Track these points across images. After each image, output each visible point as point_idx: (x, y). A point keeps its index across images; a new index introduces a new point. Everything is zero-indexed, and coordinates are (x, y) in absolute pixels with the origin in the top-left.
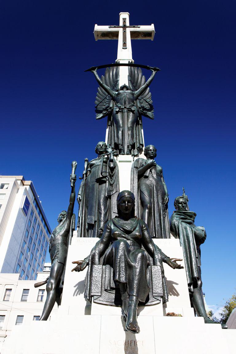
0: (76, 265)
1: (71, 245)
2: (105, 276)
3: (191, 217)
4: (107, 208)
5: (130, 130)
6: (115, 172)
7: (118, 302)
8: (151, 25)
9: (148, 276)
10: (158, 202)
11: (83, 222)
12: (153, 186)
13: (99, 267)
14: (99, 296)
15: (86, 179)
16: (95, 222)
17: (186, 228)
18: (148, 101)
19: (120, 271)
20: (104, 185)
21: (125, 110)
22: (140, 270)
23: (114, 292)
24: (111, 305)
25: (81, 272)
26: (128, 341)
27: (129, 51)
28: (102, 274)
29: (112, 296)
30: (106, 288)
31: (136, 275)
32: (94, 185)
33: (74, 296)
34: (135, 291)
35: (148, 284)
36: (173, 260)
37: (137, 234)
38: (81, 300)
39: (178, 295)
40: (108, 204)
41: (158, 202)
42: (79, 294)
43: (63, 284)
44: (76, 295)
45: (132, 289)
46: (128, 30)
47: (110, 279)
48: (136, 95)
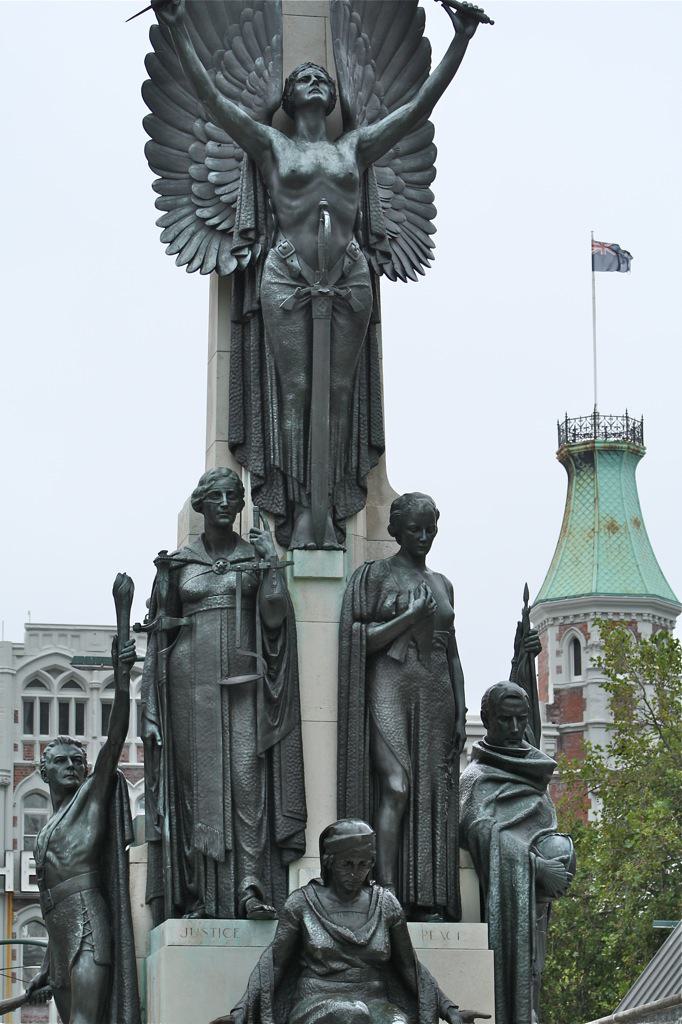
16: (227, 852)
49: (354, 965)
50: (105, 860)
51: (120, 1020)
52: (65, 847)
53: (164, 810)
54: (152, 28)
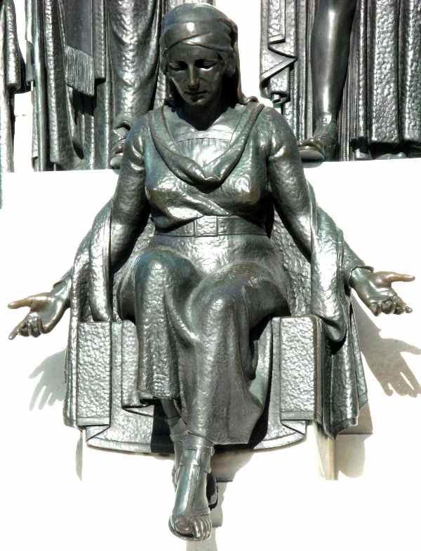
0: (26, 310)
1: (11, 168)
2: (123, 363)
4: (150, 8)
7: (162, 443)
11: (51, 65)
13: (100, 330)
14: (105, 427)
16: (99, 82)
23: (150, 411)
24: (146, 454)
25: (42, 336)
28: (111, 356)
29: (145, 424)
30: (126, 403)
33: (32, 406)
34: (201, 420)
44: (41, 407)
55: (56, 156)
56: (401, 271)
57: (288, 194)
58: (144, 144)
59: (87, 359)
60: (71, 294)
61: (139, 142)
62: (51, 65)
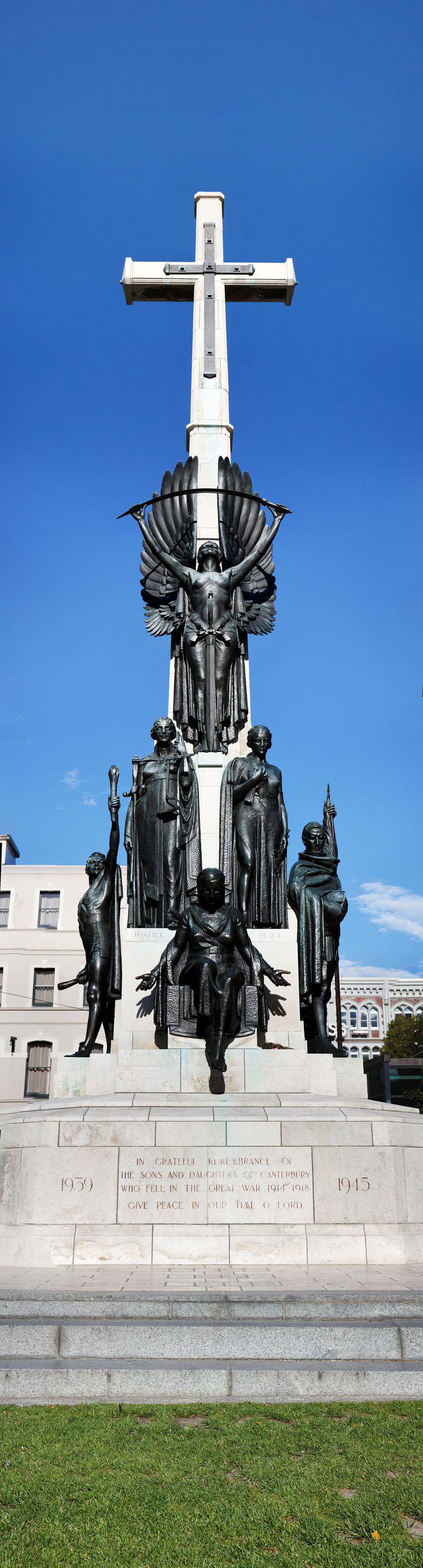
3: (329, 866)
5: (220, 688)
6: (192, 796)
8: (284, 261)
9: (239, 1002)
10: (267, 855)
11: (139, 890)
12: (261, 823)
15: (137, 804)
16: (161, 896)
17: (311, 902)
18: (168, 501)
19: (203, 1002)
20: (173, 822)
21: (211, 638)
22: (228, 1000)
25: (79, 1046)
26: (314, 1279)
27: (221, 388)
31: (223, 1006)
32: (154, 823)
33: (137, 1017)
35: (238, 1012)
36: (277, 973)
37: (227, 936)
38: (148, 1024)
39: (283, 1014)
40: (180, 860)
41: (267, 855)
42: (145, 1016)
43: (287, 837)
44: (141, 1017)
45: (218, 1023)
46: (200, 260)
47: (320, 928)
48: (235, 578)
49: (214, 945)
50: (109, 908)
51: (6, 1363)
52: (196, 957)
53: (133, 879)
54: (225, 1071)
55: (139, 923)
56: (285, 970)
57: (179, 571)
58: (188, 918)
59: (170, 999)
60: (159, 975)
61: (243, 907)
62: (139, 890)
